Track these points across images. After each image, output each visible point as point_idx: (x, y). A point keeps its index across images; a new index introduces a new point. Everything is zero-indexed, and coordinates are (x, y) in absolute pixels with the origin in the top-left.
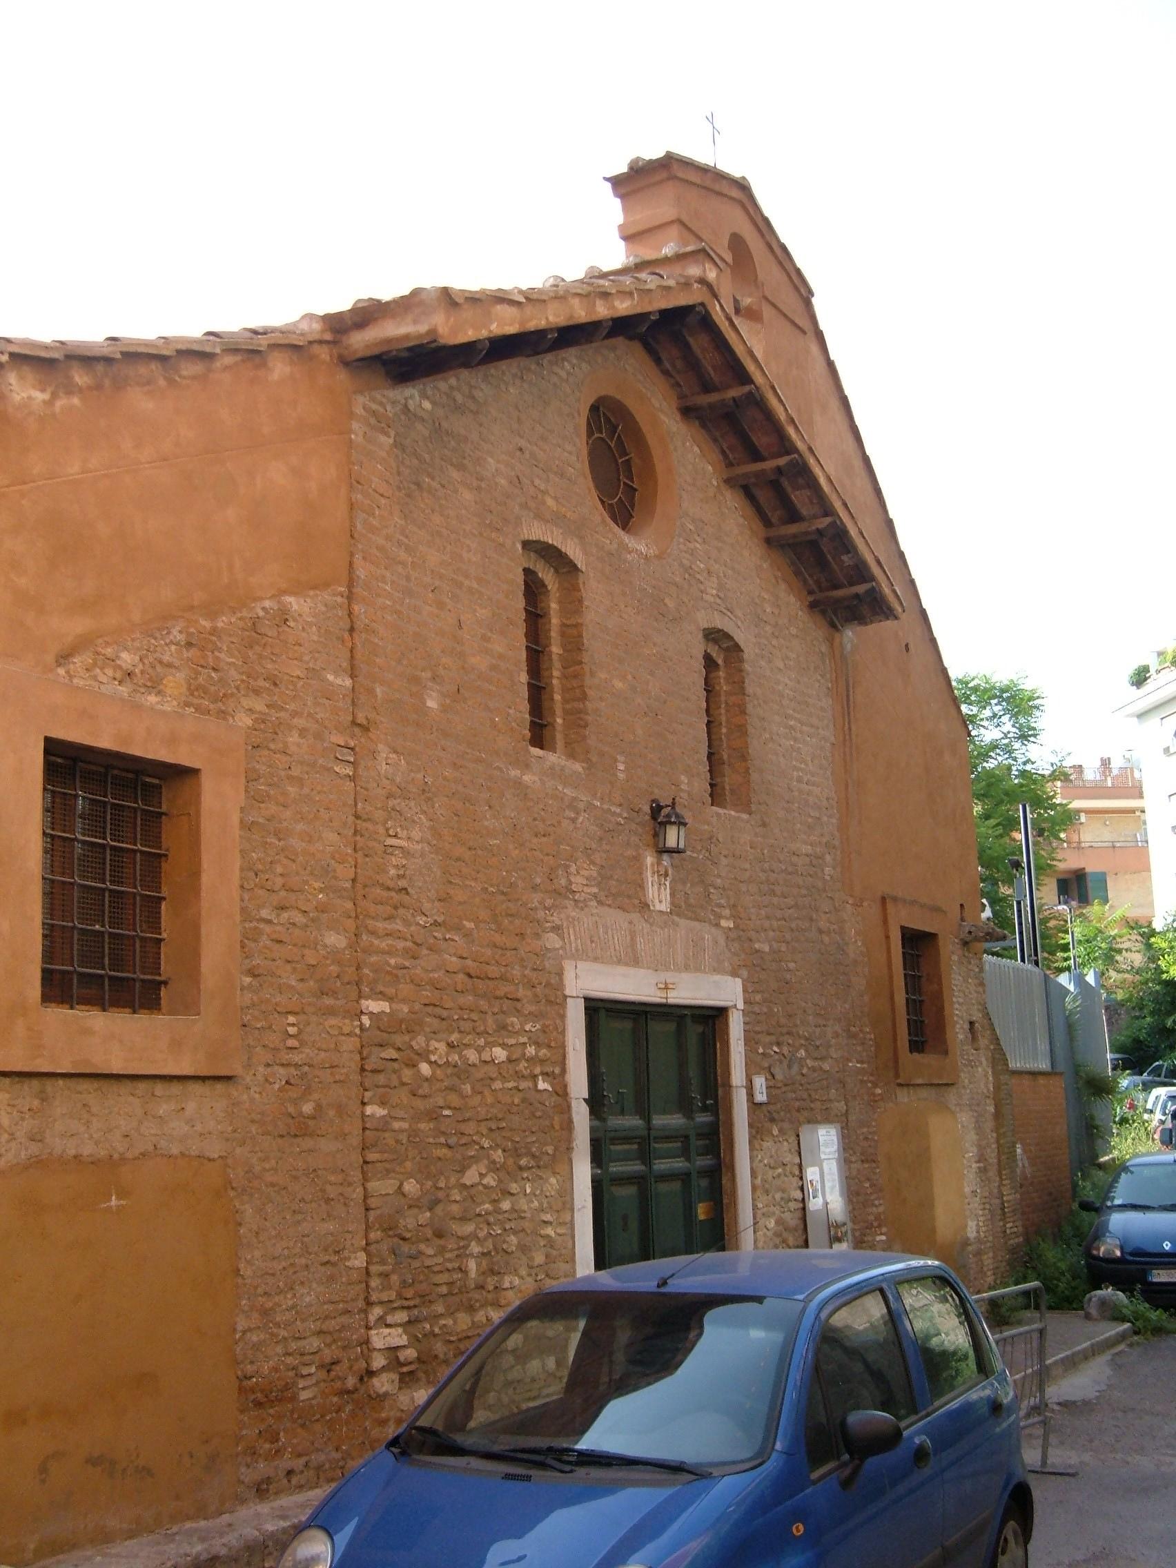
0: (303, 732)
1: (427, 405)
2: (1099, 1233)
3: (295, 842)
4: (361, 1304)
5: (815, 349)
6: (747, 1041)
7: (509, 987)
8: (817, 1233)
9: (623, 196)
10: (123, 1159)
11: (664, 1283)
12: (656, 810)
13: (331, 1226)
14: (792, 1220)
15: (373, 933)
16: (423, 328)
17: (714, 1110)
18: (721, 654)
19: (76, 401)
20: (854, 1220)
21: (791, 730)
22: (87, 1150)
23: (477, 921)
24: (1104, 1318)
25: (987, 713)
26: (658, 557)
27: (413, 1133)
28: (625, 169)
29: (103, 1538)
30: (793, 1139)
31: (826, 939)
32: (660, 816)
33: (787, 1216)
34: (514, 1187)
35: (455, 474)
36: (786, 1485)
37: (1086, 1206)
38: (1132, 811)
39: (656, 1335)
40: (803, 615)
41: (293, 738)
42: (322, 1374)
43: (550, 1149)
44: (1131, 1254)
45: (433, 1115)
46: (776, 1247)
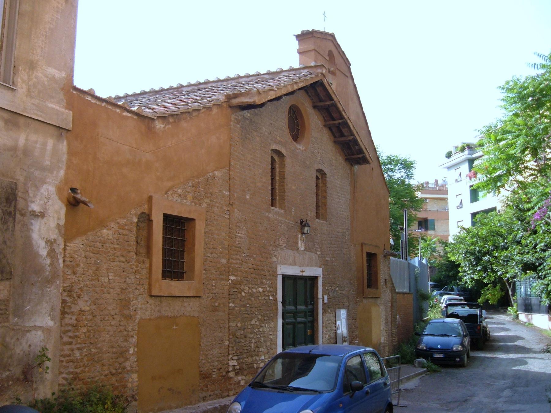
0: (218, 207)
1: (249, 115)
2: (420, 342)
3: (215, 236)
4: (227, 354)
5: (350, 81)
6: (323, 285)
7: (264, 272)
8: (339, 340)
9: (299, 41)
10: (177, 317)
11: (310, 351)
12: (302, 222)
13: (221, 334)
14: (333, 335)
15: (232, 259)
16: (252, 100)
17: (313, 305)
18: (321, 175)
19: (170, 126)
20: (349, 336)
21: (339, 198)
22: (170, 314)
23: (257, 255)
24: (419, 367)
25: (397, 168)
26: (305, 150)
27: (240, 311)
28: (300, 33)
29: (170, 408)
30: (334, 313)
31: (345, 256)
32: (303, 224)
33: (331, 334)
34: (263, 325)
35: (255, 133)
36: (339, 396)
37: (417, 334)
38: (445, 199)
39: (307, 363)
40: (343, 162)
41: (216, 209)
42: (218, 372)
43: (272, 315)
44: (429, 349)
45: (245, 306)
46: (328, 343)
